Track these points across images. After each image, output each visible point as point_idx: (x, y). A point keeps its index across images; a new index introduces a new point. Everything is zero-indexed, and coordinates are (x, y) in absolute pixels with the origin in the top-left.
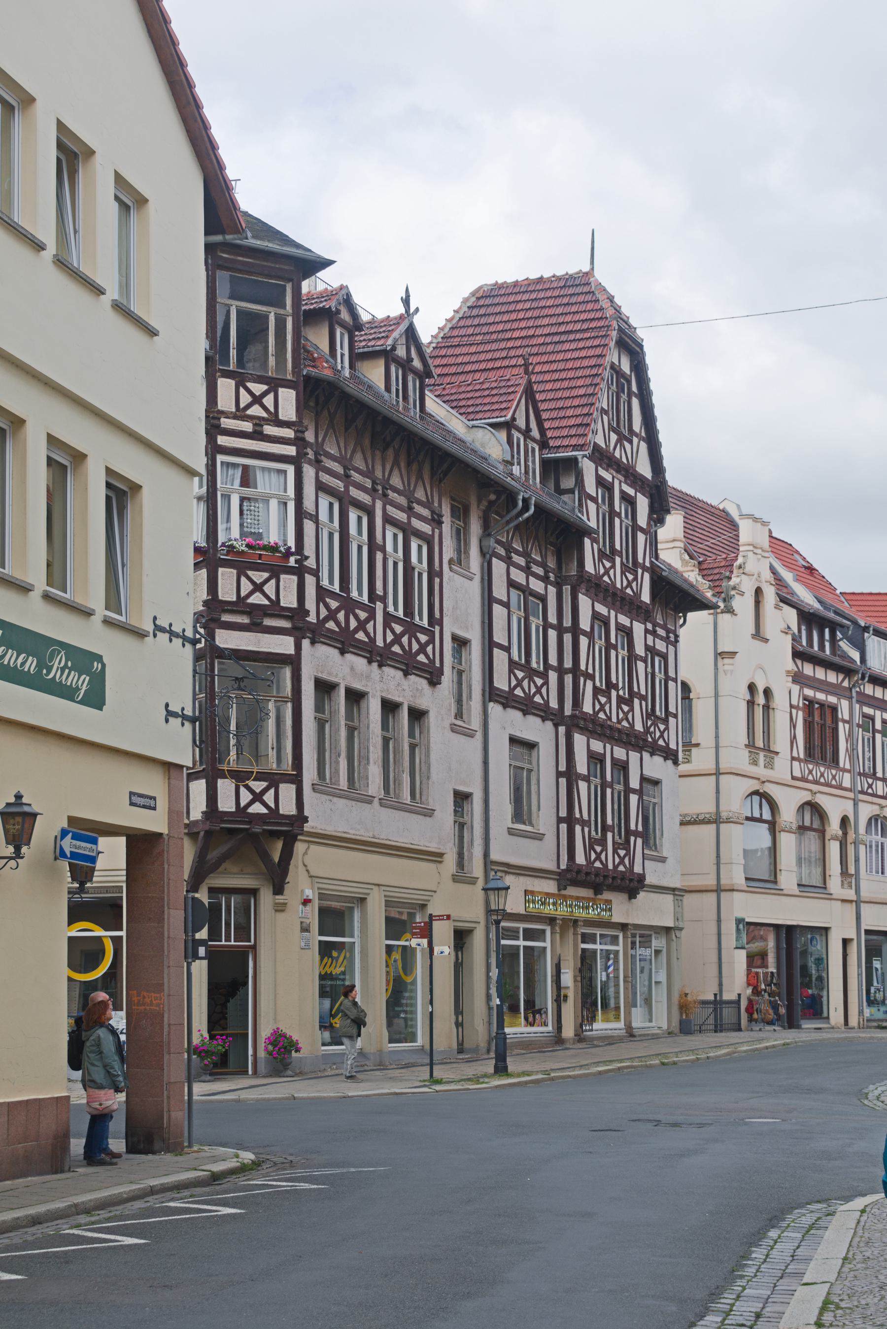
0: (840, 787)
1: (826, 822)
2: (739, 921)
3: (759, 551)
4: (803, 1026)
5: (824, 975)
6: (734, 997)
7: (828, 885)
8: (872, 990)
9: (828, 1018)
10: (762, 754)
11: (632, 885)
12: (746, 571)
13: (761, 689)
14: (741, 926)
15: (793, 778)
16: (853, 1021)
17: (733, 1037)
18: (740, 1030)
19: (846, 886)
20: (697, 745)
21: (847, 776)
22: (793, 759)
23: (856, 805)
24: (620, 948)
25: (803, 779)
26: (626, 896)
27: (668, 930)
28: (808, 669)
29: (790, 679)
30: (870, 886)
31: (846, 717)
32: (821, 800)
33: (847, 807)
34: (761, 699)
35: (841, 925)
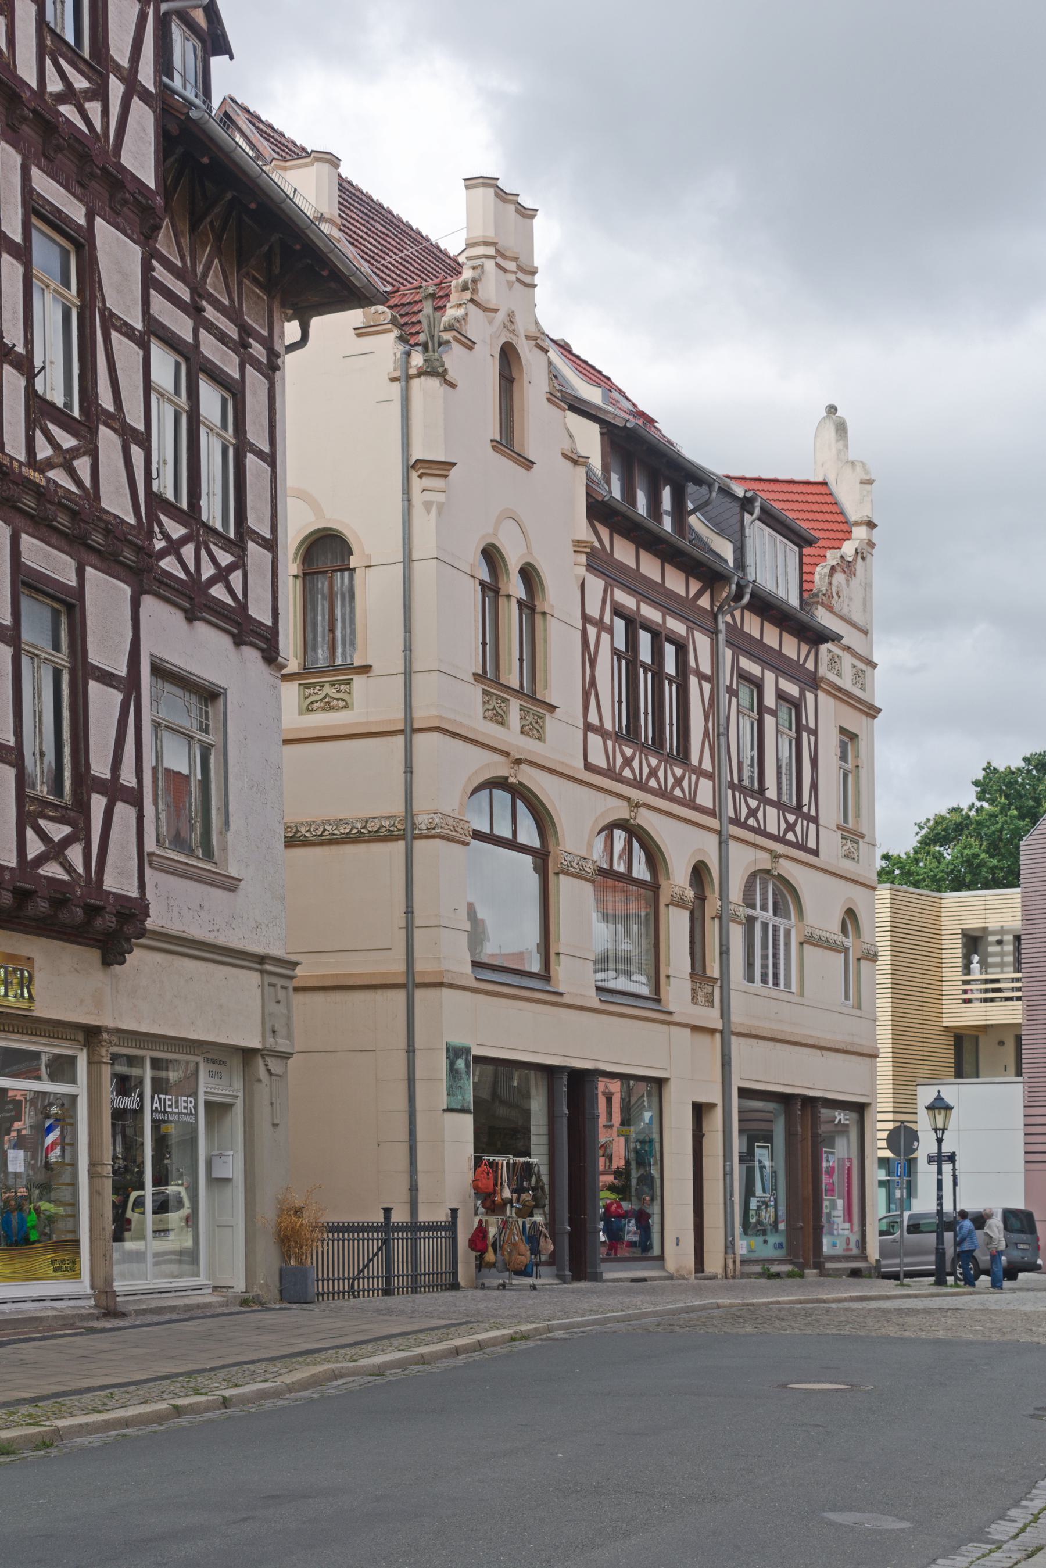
0: (690, 803)
2: (455, 1053)
3: (511, 266)
4: (607, 1276)
5: (655, 1172)
6: (442, 1216)
7: (663, 996)
8: (753, 1204)
9: (661, 1258)
10: (515, 704)
11: (110, 929)
12: (480, 297)
13: (514, 564)
14: (460, 1064)
15: (589, 767)
16: (714, 1264)
17: (437, 1302)
18: (455, 1286)
19: (701, 1000)
20: (366, 669)
21: (705, 785)
22: (588, 727)
23: (722, 844)
24: (81, 1089)
25: (609, 773)
26: (94, 956)
27: (248, 1054)
28: (624, 552)
29: (583, 559)
30: (749, 1003)
31: (706, 668)
32: (647, 820)
33: (708, 847)
34: (516, 588)
35: (691, 1075)
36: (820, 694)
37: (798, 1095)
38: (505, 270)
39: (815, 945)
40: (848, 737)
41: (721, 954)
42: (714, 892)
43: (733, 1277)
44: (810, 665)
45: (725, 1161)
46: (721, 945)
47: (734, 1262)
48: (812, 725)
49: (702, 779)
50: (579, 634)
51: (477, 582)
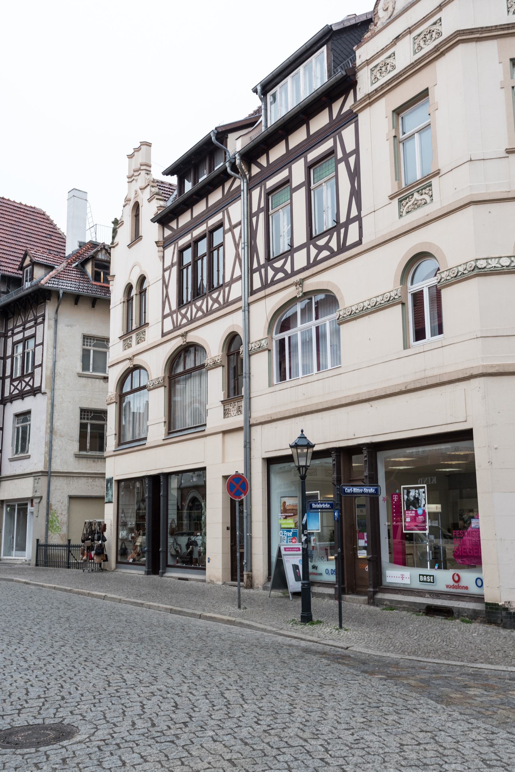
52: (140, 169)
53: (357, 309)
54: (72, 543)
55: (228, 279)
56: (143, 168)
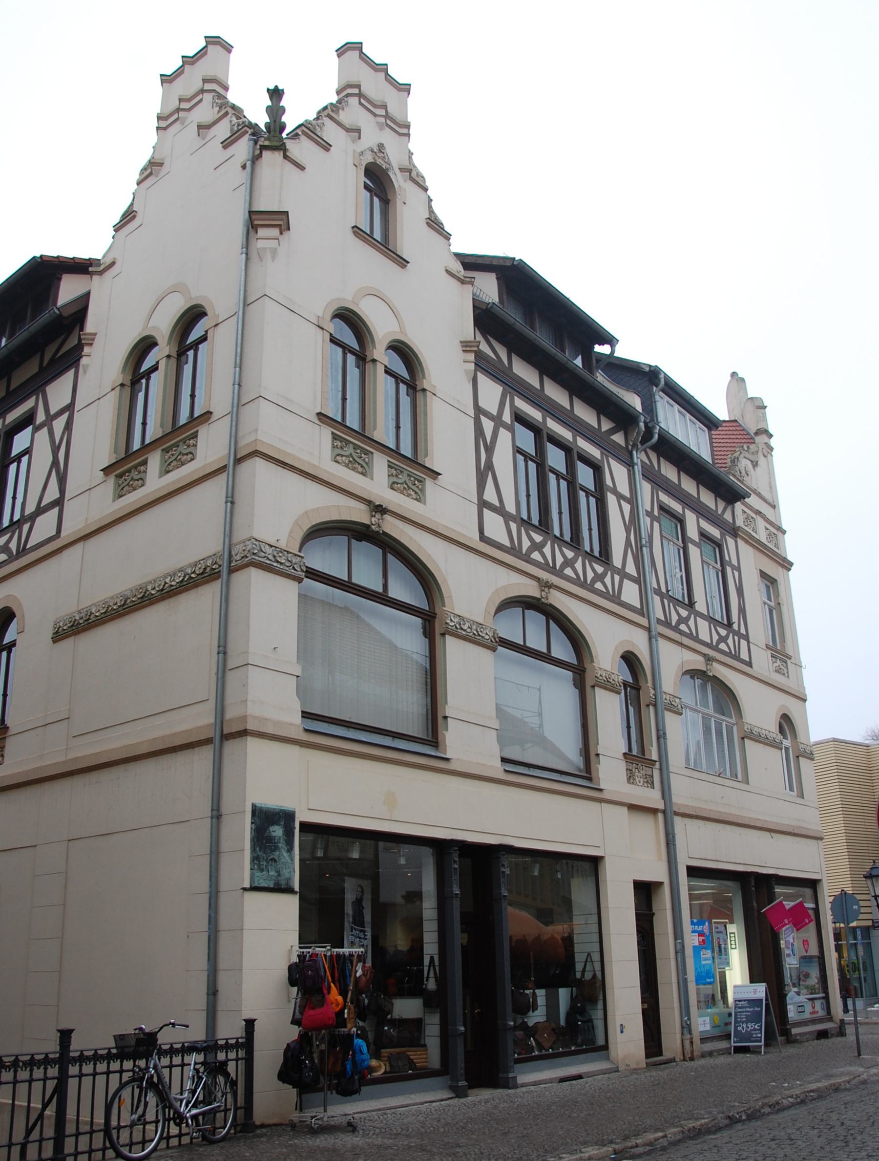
1: (585, 654)
2: (264, 819)
4: (522, 1079)
9: (606, 1047)
22: (483, 504)
25: (514, 551)
35: (630, 855)
36: (739, 540)
37: (752, 873)
38: (375, 115)
39: (756, 741)
40: (769, 581)
41: (658, 738)
42: (647, 682)
43: (692, 1059)
44: (728, 516)
45: (676, 939)
46: (658, 730)
47: (692, 1043)
48: (734, 562)
49: (625, 581)
50: (471, 423)
51: (328, 337)
52: (202, 91)
53: (154, 588)
54: (77, 1045)
55: (30, 508)
56: (208, 86)
